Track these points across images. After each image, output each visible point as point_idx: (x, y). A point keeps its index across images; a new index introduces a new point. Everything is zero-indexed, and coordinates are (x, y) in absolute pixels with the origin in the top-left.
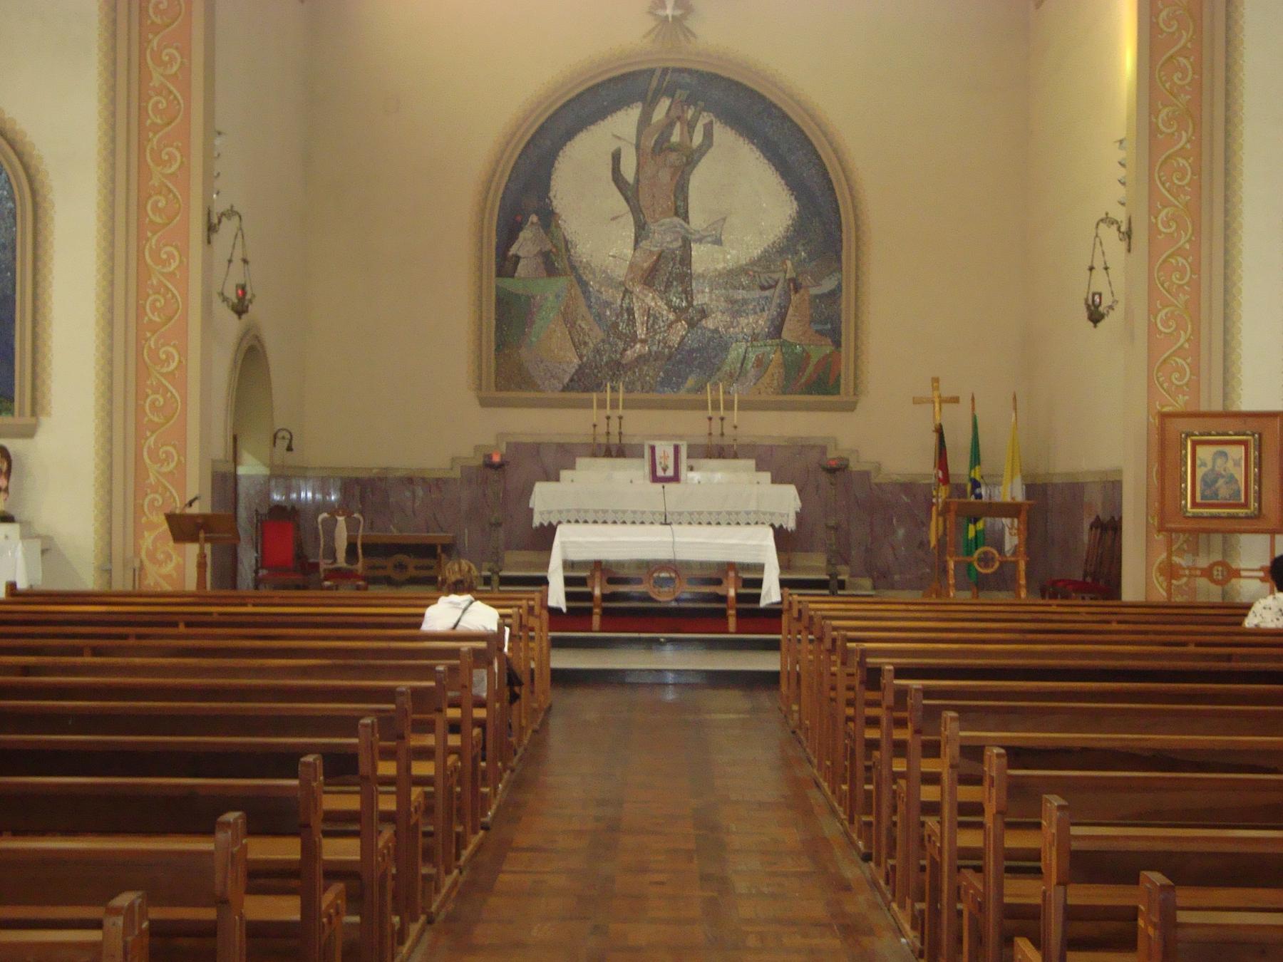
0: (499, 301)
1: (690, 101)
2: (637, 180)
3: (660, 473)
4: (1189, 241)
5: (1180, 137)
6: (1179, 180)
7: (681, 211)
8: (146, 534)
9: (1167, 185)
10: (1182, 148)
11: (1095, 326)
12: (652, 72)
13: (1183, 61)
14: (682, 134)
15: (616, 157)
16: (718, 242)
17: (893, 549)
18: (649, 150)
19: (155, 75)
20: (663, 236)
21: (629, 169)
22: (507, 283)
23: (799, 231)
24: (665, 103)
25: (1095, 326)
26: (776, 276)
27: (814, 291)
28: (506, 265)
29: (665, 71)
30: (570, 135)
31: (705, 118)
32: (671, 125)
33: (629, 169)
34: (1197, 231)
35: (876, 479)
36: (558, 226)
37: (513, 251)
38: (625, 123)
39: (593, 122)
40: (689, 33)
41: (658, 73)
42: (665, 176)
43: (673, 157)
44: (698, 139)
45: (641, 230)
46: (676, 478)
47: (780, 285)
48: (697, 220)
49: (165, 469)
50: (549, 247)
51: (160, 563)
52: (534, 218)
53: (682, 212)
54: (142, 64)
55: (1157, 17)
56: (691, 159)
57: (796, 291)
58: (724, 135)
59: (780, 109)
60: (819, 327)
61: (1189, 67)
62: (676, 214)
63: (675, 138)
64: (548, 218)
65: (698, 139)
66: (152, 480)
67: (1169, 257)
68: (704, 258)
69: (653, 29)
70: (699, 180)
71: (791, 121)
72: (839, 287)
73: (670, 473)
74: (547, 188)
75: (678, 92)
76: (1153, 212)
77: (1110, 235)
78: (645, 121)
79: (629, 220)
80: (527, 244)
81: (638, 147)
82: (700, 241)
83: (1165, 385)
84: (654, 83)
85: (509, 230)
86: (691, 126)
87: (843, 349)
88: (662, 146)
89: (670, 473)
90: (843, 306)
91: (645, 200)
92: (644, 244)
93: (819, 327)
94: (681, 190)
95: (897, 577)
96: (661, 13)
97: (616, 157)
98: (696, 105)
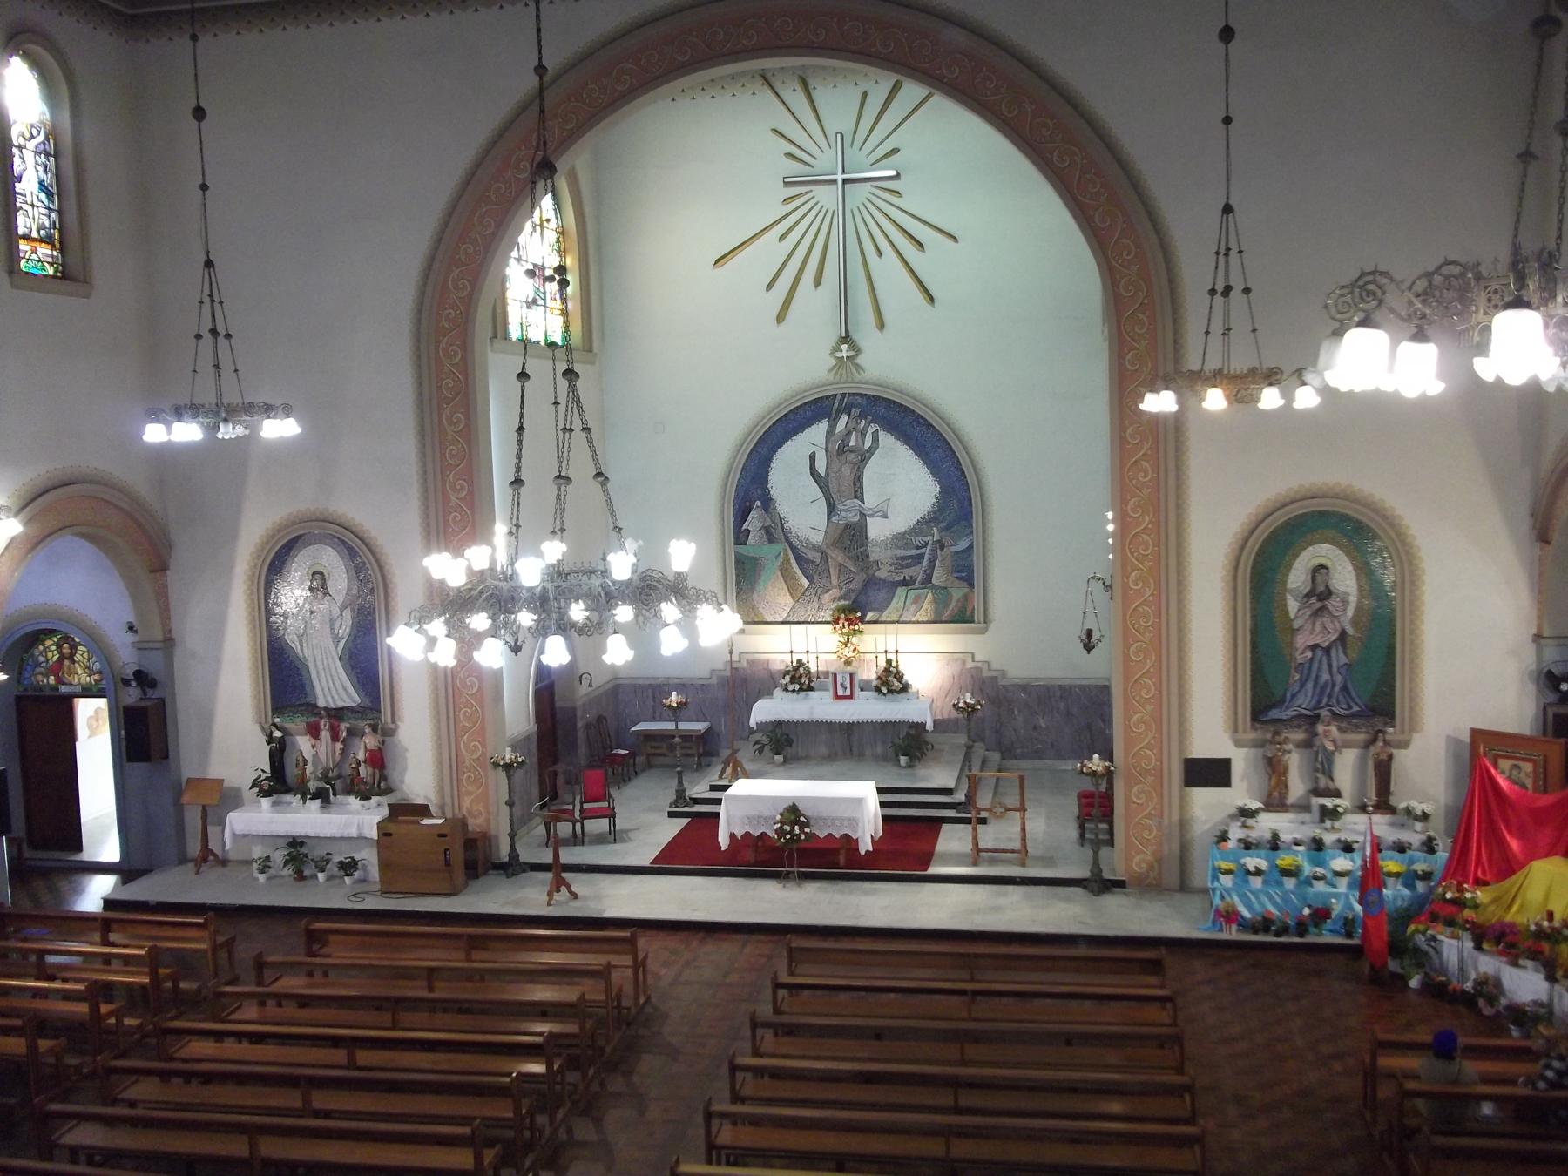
0: (738, 561)
1: (862, 416)
2: (827, 474)
3: (840, 693)
4: (1152, 594)
5: (1144, 520)
6: (1145, 550)
7: (859, 494)
8: (466, 798)
9: (1136, 554)
10: (1145, 528)
11: (1362, 269)
12: (835, 396)
13: (1144, 463)
14: (857, 440)
15: (812, 458)
16: (885, 516)
17: (1015, 730)
18: (835, 452)
19: (453, 498)
20: (846, 513)
21: (821, 467)
22: (742, 549)
23: (945, 493)
24: (845, 418)
25: (1362, 269)
26: (926, 539)
27: (954, 549)
28: (741, 537)
29: (843, 395)
30: (780, 444)
31: (873, 428)
32: (849, 433)
33: (821, 467)
34: (1158, 584)
35: (1001, 683)
36: (775, 508)
37: (745, 526)
38: (816, 433)
39: (795, 434)
40: (858, 367)
41: (839, 397)
42: (847, 471)
43: (851, 457)
44: (868, 443)
45: (831, 508)
46: (851, 697)
47: (929, 546)
48: (870, 500)
49: (475, 757)
50: (768, 523)
51: (475, 817)
52: (758, 503)
53: (858, 494)
54: (444, 492)
55: (1125, 432)
56: (864, 457)
57: (942, 549)
58: (886, 439)
59: (925, 420)
60: (958, 575)
61: (1149, 468)
62: (856, 497)
63: (852, 443)
64: (768, 503)
65: (868, 443)
66: (467, 763)
67: (1138, 605)
68: (877, 530)
69: (834, 366)
70: (870, 472)
71: (934, 427)
72: (971, 547)
73: (848, 693)
74: (767, 482)
75: (853, 410)
76: (1126, 575)
77: (1097, 587)
78: (831, 432)
79: (823, 503)
80: (754, 522)
81: (827, 450)
82: (871, 516)
83: (1137, 698)
84: (836, 405)
85: (742, 513)
86: (863, 434)
87: (975, 590)
88: (843, 449)
89: (848, 693)
90: (975, 559)
91: (833, 488)
92: (834, 519)
93: (958, 575)
94: (858, 479)
95: (1019, 751)
96: (839, 354)
97: (812, 458)
98: (866, 419)
